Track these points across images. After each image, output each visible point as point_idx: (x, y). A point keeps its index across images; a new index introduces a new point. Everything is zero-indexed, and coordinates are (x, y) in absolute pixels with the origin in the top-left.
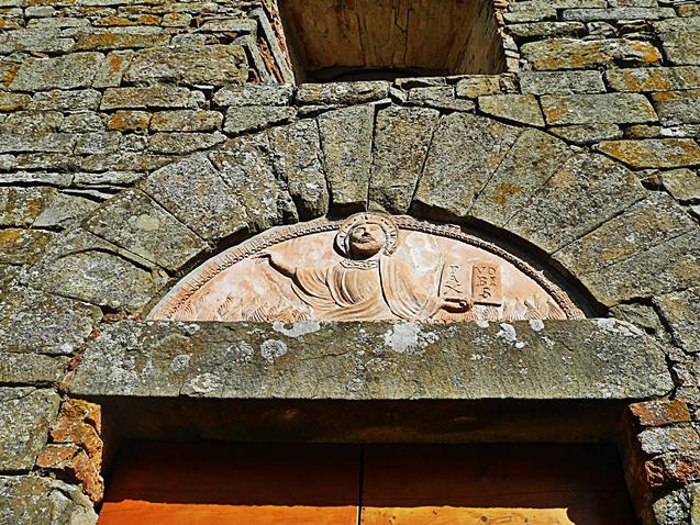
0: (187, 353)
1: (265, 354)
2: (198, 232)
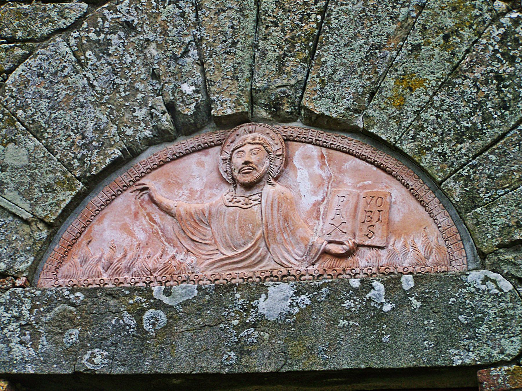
0: (75, 327)
1: (147, 327)
2: (70, 167)
